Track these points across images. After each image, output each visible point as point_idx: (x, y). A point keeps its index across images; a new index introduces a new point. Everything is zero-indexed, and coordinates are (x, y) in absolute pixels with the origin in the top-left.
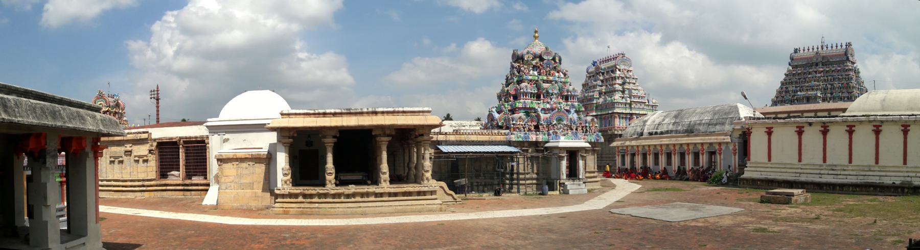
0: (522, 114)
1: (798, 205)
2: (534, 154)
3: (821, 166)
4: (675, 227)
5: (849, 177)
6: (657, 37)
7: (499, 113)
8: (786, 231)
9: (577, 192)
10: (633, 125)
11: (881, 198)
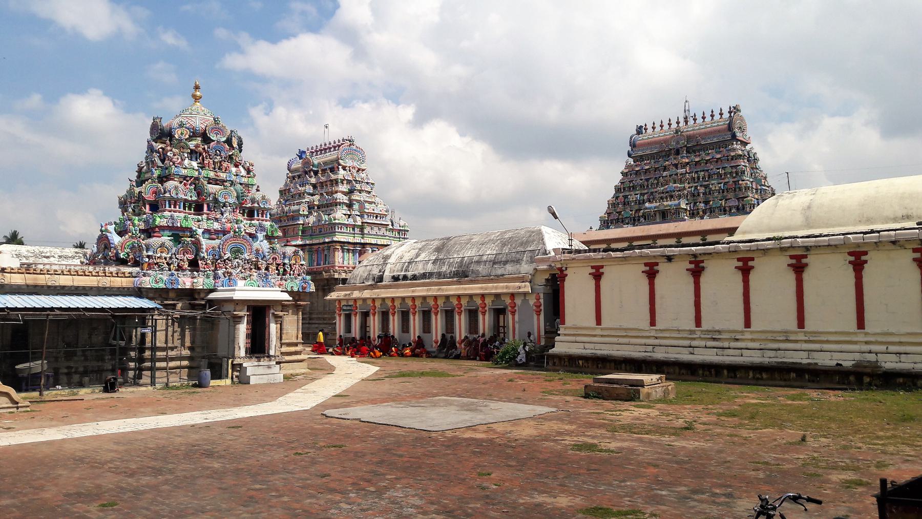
0: (166, 239)
1: (651, 402)
2: (187, 313)
3: (692, 332)
4: (436, 440)
5: (745, 352)
6: (408, 112)
7: (121, 234)
8: (632, 451)
9: (264, 380)
10: (365, 263)
11: (814, 394)
